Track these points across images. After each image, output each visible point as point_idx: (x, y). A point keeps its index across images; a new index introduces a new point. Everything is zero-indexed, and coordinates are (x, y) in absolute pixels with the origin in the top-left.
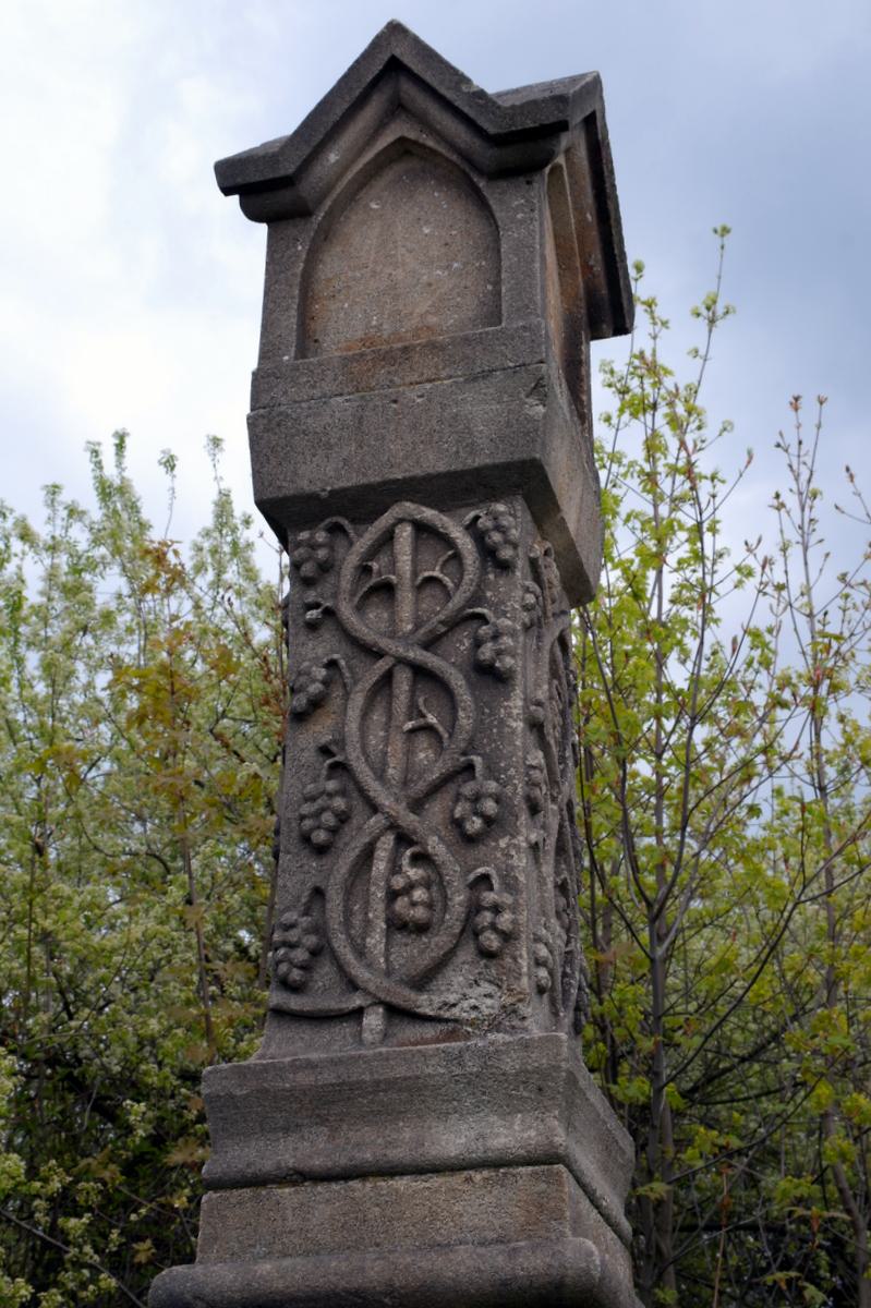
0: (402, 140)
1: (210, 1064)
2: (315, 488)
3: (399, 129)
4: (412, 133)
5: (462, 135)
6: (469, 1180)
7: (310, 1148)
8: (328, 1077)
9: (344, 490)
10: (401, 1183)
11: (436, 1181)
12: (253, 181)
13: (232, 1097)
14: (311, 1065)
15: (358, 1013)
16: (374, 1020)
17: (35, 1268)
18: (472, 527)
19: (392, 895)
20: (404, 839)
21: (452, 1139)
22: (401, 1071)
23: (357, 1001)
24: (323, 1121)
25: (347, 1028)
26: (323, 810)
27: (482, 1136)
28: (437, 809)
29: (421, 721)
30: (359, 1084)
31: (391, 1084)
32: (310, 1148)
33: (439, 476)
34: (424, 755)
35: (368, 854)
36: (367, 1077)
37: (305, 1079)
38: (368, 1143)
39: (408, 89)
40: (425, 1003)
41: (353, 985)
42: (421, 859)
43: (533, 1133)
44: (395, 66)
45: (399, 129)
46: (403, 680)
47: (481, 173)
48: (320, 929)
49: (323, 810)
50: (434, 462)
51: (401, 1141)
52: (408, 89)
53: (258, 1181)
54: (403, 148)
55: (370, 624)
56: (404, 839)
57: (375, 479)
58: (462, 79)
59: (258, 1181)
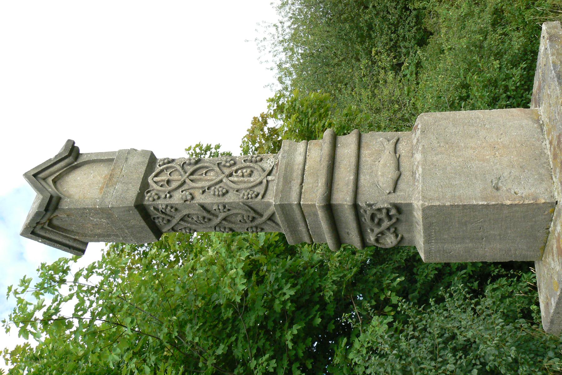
0: (53, 180)
2: (137, 192)
4: (53, 177)
5: (62, 164)
6: (308, 156)
8: (281, 180)
9: (140, 187)
10: (306, 167)
11: (307, 161)
12: (47, 202)
13: (281, 198)
14: (278, 182)
15: (267, 181)
16: (270, 178)
18: (160, 166)
19: (243, 176)
21: (299, 159)
22: (284, 167)
23: (265, 181)
24: (291, 182)
25: (270, 185)
26: (218, 190)
27: (300, 154)
29: (204, 174)
30: (285, 174)
31: (286, 168)
33: (146, 169)
34: (212, 174)
35: (232, 182)
36: (283, 173)
37: (281, 184)
41: (261, 183)
42: (236, 171)
43: (301, 146)
44: (35, 175)
45: (50, 180)
46: (192, 177)
47: (73, 163)
48: (246, 189)
49: (218, 190)
50: (143, 169)
53: (301, 193)
56: (231, 175)
57: (141, 180)
58: (50, 160)
59: (301, 193)
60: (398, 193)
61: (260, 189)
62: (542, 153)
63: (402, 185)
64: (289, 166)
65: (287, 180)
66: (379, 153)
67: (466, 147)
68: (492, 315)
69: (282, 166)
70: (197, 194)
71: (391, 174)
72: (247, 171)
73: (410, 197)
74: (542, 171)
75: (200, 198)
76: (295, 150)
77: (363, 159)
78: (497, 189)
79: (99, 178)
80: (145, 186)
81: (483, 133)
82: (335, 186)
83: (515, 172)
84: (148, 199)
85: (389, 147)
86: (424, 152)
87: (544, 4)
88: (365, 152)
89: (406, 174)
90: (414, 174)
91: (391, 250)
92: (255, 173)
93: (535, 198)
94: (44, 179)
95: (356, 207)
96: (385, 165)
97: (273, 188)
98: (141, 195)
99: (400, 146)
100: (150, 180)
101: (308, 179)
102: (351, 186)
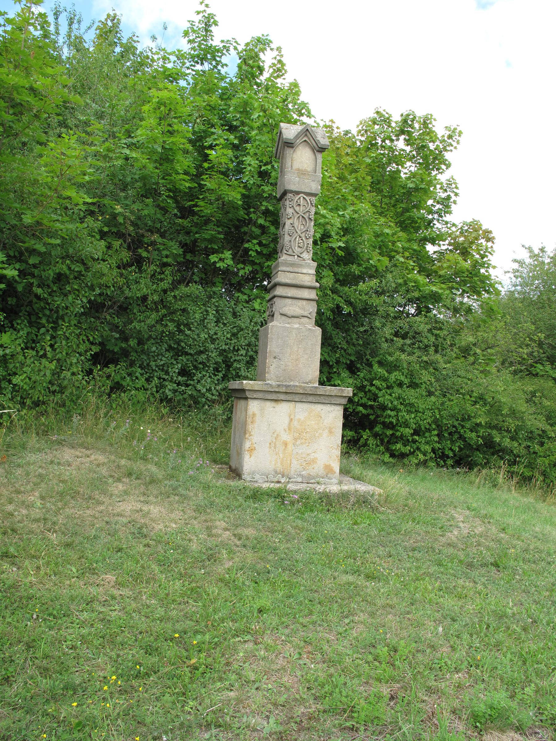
1: (163, 236)
3: (305, 139)
5: (315, 144)
7: (290, 269)
16: (296, 257)
17: (40, 254)
20: (300, 237)
21: (305, 271)
28: (304, 234)
32: (290, 269)
34: (302, 227)
38: (296, 270)
39: (308, 134)
40: (301, 256)
45: (305, 139)
48: (291, 245)
50: (307, 190)
51: (300, 270)
52: (308, 134)
54: (305, 141)
55: (297, 209)
56: (300, 237)
60: (279, 316)
61: (290, 252)
62: (292, 380)
63: (284, 318)
64: (300, 266)
65: (292, 265)
66: (304, 309)
67: (299, 348)
68: (153, 323)
69: (303, 263)
70: (291, 221)
71: (290, 313)
72: (302, 244)
73: (277, 321)
74: (282, 379)
75: (288, 222)
76: (311, 269)
77: (300, 301)
78: (275, 358)
79: (306, 166)
80: (298, 193)
81: (306, 357)
82: (286, 288)
83: (283, 367)
84: (289, 195)
85: (306, 314)
86: (297, 328)
87: (250, 350)
88: (304, 302)
89: (290, 320)
90: (288, 323)
91: (339, 338)
92: (300, 249)
93: (268, 373)
94: (306, 135)
95: (274, 297)
96: (295, 311)
97: (290, 258)
98: (291, 192)
99: (306, 319)
100: (301, 195)
101: (292, 275)
102: (285, 295)
